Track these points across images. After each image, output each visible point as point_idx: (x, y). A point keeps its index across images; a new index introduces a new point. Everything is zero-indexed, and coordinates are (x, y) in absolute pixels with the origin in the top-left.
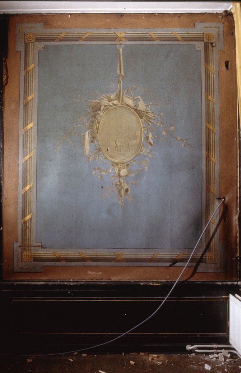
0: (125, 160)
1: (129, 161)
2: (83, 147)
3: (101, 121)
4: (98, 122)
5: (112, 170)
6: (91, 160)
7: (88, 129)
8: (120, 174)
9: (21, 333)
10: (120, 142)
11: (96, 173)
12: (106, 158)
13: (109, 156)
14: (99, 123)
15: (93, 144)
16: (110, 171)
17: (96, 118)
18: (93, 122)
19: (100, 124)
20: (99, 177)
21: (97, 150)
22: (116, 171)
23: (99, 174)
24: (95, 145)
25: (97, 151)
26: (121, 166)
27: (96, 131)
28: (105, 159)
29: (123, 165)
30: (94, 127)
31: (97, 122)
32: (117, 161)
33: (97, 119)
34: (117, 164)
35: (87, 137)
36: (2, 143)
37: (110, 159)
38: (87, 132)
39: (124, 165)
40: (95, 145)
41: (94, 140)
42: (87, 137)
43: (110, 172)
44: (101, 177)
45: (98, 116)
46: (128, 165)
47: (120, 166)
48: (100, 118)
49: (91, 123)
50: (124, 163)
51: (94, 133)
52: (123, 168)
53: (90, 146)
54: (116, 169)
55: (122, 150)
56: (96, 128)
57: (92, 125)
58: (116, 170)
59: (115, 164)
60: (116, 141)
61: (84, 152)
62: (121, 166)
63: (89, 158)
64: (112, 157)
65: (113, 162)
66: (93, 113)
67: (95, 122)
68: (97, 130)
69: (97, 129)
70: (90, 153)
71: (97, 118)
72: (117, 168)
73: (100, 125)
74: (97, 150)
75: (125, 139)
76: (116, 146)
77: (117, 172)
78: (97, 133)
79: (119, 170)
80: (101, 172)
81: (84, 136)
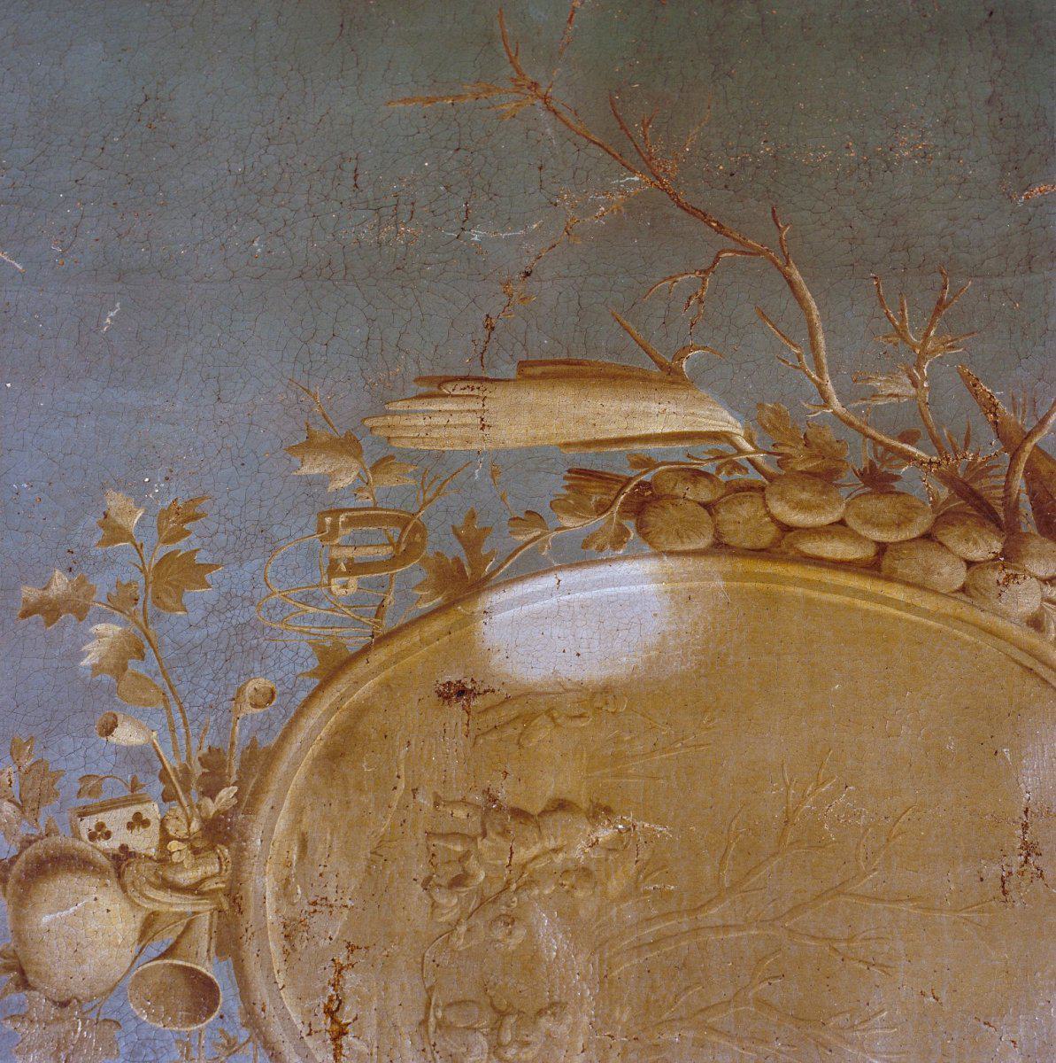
0: (275, 946)
1: (252, 1019)
2: (510, 370)
3: (897, 592)
4: (882, 548)
5: (140, 757)
6: (313, 467)
7: (771, 425)
8: (63, 885)
9: (18, 266)
10: (585, 872)
11: (114, 533)
12: (334, 666)
13: (360, 712)
14: (876, 565)
15: (556, 485)
16: (127, 735)
17: (945, 518)
18: (877, 481)
19: (867, 585)
20: (60, 584)
21: (455, 550)
22: (116, 820)
23: (103, 584)
24: (532, 517)
25: (442, 543)
26: (194, 889)
27: (742, 519)
28: (323, 653)
29: (204, 922)
30: (801, 506)
31: (877, 535)
32: (272, 830)
33: (927, 537)
34: (218, 832)
35: (657, 415)
36: (527, 718)
37: (318, 725)
38: (719, 419)
39: (202, 938)
40: (532, 517)
41: (602, 508)
42: (657, 415)
43: (108, 730)
44: (50, 611)
45: (986, 546)
46: (203, 994)
47: (186, 877)
48: (951, 574)
49: (861, 456)
50: (229, 942)
51: (708, 507)
52: (149, 926)
53: (531, 458)
54: (152, 811)
55: (450, 903)
56: (786, 529)
57: (825, 478)
58: (139, 821)
59: (227, 795)
60: (600, 812)
61: (436, 385)
62: (194, 889)
63: (348, 445)
64: (335, 756)
65: (260, 760)
66: (1019, 482)
67: (881, 506)
68: (768, 535)
69: (783, 544)
70: (414, 457)
71: (951, 537)
72: (166, 838)
73: (842, 579)
74: (455, 550)
75: (638, 948)
76: (519, 814)
77: (101, 832)
78: (720, 546)
79: (124, 857)
80: (122, 601)
81: (670, 377)
